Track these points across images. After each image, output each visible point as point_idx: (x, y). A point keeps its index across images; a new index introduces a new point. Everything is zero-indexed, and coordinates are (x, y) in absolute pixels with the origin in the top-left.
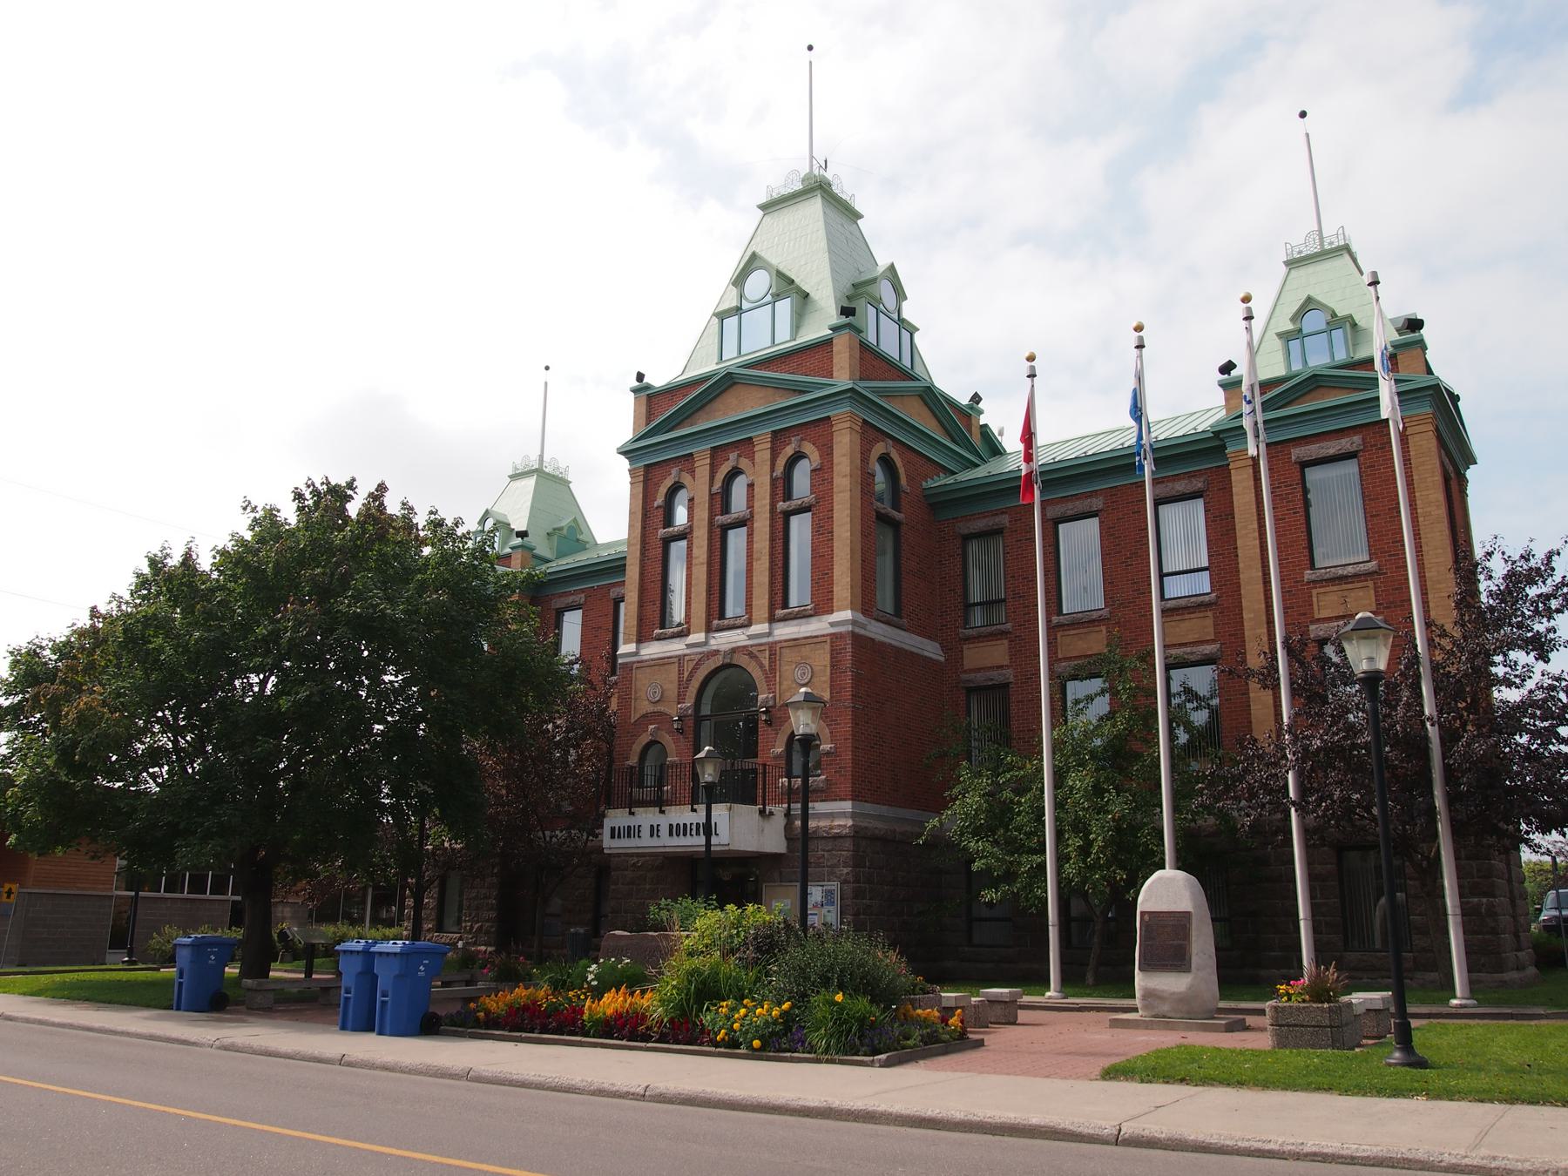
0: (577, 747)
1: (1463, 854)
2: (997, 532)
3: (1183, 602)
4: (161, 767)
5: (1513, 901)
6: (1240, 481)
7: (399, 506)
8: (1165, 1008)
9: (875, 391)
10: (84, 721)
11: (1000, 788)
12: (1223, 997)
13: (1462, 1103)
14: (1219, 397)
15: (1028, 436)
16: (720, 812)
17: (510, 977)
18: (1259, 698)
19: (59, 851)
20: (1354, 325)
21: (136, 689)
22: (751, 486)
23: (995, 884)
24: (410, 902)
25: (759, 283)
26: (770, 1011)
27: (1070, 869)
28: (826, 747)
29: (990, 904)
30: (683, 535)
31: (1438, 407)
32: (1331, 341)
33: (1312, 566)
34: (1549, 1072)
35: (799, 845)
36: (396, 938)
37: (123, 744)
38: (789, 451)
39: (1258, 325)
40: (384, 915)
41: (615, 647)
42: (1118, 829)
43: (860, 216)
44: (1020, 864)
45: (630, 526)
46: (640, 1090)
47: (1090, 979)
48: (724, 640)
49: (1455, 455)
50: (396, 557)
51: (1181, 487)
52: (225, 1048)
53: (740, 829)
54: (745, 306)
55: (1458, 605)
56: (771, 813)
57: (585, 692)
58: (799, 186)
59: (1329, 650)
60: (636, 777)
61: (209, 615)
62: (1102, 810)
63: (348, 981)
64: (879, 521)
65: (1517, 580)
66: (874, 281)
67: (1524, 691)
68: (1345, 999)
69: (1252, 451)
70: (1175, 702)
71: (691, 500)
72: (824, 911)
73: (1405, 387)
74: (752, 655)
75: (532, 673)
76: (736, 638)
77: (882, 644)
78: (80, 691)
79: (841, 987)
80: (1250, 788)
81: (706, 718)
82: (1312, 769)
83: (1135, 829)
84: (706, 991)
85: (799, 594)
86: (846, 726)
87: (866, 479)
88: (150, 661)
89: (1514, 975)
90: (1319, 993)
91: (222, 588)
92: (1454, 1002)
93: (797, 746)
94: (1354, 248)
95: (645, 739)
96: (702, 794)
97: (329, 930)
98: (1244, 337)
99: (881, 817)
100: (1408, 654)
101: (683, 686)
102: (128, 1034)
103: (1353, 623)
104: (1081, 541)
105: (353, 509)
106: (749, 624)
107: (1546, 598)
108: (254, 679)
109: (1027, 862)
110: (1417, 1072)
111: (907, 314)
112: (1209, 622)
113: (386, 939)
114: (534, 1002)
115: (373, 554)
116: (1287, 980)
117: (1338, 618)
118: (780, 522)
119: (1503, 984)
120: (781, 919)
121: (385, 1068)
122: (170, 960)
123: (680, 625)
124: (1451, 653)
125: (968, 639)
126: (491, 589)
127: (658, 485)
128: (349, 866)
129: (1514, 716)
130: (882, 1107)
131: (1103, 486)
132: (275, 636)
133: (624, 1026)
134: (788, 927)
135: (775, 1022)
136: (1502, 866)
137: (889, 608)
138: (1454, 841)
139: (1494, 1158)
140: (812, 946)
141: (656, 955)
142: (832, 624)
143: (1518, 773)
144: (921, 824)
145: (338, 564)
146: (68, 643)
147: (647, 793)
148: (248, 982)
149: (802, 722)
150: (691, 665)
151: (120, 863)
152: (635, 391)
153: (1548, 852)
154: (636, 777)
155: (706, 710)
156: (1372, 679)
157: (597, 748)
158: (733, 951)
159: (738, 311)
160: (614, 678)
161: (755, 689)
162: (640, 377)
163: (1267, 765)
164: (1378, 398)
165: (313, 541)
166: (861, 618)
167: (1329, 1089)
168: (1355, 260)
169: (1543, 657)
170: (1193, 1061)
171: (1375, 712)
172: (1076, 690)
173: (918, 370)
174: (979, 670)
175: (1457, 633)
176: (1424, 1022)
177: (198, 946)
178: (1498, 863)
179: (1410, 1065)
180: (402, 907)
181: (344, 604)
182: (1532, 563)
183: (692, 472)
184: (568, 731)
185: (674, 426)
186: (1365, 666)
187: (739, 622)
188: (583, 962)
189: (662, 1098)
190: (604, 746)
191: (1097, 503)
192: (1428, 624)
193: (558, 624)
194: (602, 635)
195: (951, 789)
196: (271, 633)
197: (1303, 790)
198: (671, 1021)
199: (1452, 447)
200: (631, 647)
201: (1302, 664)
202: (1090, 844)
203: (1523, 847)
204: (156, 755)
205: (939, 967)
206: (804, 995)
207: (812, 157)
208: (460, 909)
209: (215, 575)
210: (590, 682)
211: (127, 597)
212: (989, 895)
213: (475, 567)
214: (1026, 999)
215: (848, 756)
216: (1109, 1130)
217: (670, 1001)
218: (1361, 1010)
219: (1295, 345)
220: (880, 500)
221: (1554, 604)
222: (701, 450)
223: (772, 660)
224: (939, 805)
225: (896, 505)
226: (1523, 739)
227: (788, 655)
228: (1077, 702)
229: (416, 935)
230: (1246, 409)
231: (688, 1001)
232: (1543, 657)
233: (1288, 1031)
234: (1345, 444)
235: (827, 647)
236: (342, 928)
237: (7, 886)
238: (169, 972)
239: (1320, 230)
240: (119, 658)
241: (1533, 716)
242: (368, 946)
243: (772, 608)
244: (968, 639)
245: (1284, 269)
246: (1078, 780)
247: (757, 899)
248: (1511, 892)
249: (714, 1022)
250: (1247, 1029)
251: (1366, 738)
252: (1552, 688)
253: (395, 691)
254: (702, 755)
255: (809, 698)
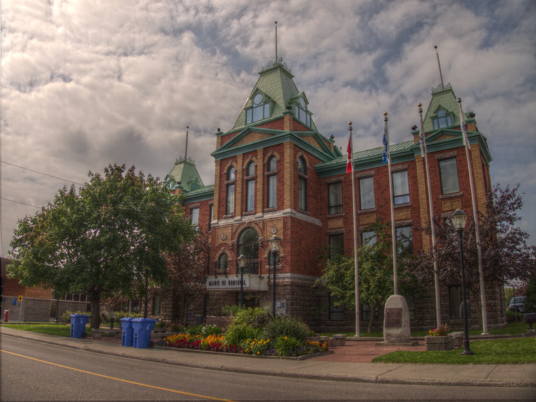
0: (198, 255)
1: (487, 286)
2: (339, 182)
3: (401, 206)
4: (64, 259)
5: (501, 301)
6: (419, 166)
7: (139, 174)
8: (393, 339)
9: (299, 135)
10: (41, 244)
11: (340, 268)
12: (412, 335)
13: (483, 365)
14: (412, 138)
15: (350, 150)
16: (246, 277)
17: (176, 330)
18: (425, 238)
19: (34, 286)
20: (454, 115)
21: (57, 234)
22: (256, 166)
23: (338, 300)
24: (143, 305)
25: (258, 99)
26: (263, 342)
27: (363, 295)
28: (282, 255)
29: (337, 307)
30: (234, 183)
31: (480, 141)
32: (447, 120)
33: (442, 194)
34: (509, 354)
35: (272, 288)
36: (139, 317)
37: (52, 251)
38: (269, 154)
39: (424, 114)
40: (135, 309)
41: (210, 220)
42: (379, 282)
43: (293, 77)
44: (346, 294)
45: (216, 180)
46: (220, 367)
47: (369, 331)
48: (247, 219)
49: (485, 157)
50: (138, 190)
51: (400, 167)
52: (87, 350)
53: (252, 282)
54: (254, 106)
55: (487, 206)
56: (263, 277)
57: (200, 237)
58: (272, 67)
59: (447, 222)
60: (218, 265)
61: (78, 210)
62: (374, 275)
63: (124, 330)
64: (300, 178)
65: (504, 199)
66: (297, 98)
67: (506, 234)
68: (449, 334)
69: (423, 156)
70: (398, 239)
71: (236, 171)
72: (281, 310)
73: (470, 136)
74: (256, 224)
75: (181, 230)
76: (251, 218)
77: (301, 220)
78: (40, 235)
79: (287, 334)
80: (422, 267)
81: (241, 245)
82: (442, 261)
83: (384, 281)
84: (241, 336)
85: (273, 202)
86: (288, 249)
87: (295, 164)
88: (60, 225)
89: (501, 324)
90: (442, 333)
91: (83, 201)
92: (483, 334)
93: (272, 255)
94: (454, 90)
95: (220, 252)
96: (240, 271)
97: (118, 314)
98: (420, 118)
99: (299, 277)
100: (472, 223)
101: (233, 234)
102: (57, 344)
103: (455, 212)
104: (368, 185)
105: (124, 175)
106: (256, 213)
107: (513, 204)
108: (93, 231)
109: (349, 293)
110: (471, 355)
111: (309, 108)
112: (409, 212)
113: (136, 317)
114: (185, 338)
115: (130, 190)
116: (432, 329)
117: (450, 211)
118: (266, 179)
119: (497, 327)
120: (266, 312)
121: (137, 358)
122: (69, 321)
123: (232, 214)
124: (485, 222)
125: (330, 219)
126: (169, 201)
127: (224, 166)
128: (124, 293)
129: (503, 243)
130: (300, 373)
131: (373, 166)
132: (99, 217)
133: (214, 347)
134: (269, 315)
135: (264, 346)
136: (498, 290)
137: (303, 208)
138: (485, 283)
139: (492, 381)
140: (277, 321)
141: (223, 324)
142: (284, 214)
143: (504, 261)
144: (314, 281)
145: (119, 193)
146: (36, 219)
147: (221, 270)
148: (93, 330)
149: (274, 247)
150: (236, 227)
151: (52, 290)
152: (217, 134)
153: (512, 286)
154: (218, 265)
155: (241, 242)
156: (460, 231)
157: (204, 255)
158: (250, 323)
159: (252, 107)
160: (210, 232)
161: (258, 235)
162: (219, 130)
163: (427, 260)
164: (462, 139)
165: (111, 186)
166: (294, 211)
167: (444, 363)
168: (453, 94)
169: (512, 223)
170: (401, 356)
171: (461, 241)
172: (366, 235)
173: (313, 127)
174: (334, 229)
175: (486, 216)
176: (473, 340)
177: (78, 318)
178: (497, 290)
179: (468, 354)
180: (141, 307)
181: (121, 206)
182: (509, 193)
183: (236, 162)
184: (195, 249)
185: (230, 146)
186: (458, 226)
187: (252, 213)
188: (201, 326)
189: (227, 370)
190: (207, 255)
191: (373, 172)
192: (478, 212)
193: (191, 213)
194: (207, 216)
195: (324, 269)
196: (98, 216)
197: (439, 268)
198: (230, 345)
199: (485, 155)
200: (216, 221)
201: (439, 226)
202: (370, 287)
203: (505, 284)
204: (62, 256)
205: (318, 325)
206: (274, 337)
207: (277, 57)
208: (160, 308)
209: (80, 197)
210: (202, 233)
211: (53, 204)
212: (336, 304)
213: (163, 194)
214: (348, 337)
215: (289, 258)
216: (373, 378)
217: (229, 339)
218: (454, 338)
219: (435, 121)
220: (300, 171)
221: (515, 206)
222: (240, 154)
223: (263, 226)
224: (320, 275)
225: (305, 173)
226: (506, 250)
227: (269, 224)
228: (366, 239)
229: (145, 316)
230: (421, 141)
231: (235, 339)
232: (512, 223)
233: (432, 345)
234: (452, 154)
235: (282, 221)
236: (122, 313)
237: (20, 296)
238: (69, 325)
239: (442, 84)
240: (51, 224)
241: (509, 242)
242: (130, 319)
243: (263, 207)
244: (330, 219)
245: (431, 96)
246: (366, 266)
247: (258, 305)
248: (501, 298)
249: (244, 346)
250: (418, 345)
251: (458, 250)
252: (514, 233)
253: (137, 235)
254: (239, 258)
255: (276, 239)
